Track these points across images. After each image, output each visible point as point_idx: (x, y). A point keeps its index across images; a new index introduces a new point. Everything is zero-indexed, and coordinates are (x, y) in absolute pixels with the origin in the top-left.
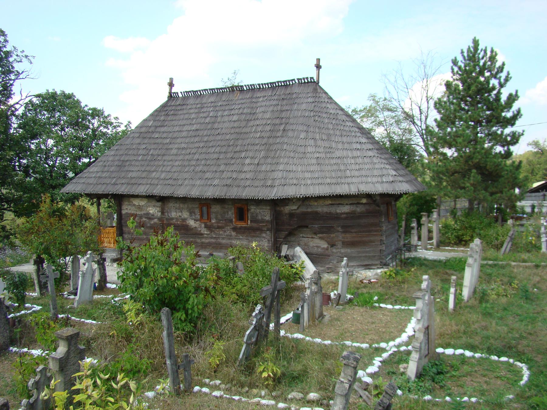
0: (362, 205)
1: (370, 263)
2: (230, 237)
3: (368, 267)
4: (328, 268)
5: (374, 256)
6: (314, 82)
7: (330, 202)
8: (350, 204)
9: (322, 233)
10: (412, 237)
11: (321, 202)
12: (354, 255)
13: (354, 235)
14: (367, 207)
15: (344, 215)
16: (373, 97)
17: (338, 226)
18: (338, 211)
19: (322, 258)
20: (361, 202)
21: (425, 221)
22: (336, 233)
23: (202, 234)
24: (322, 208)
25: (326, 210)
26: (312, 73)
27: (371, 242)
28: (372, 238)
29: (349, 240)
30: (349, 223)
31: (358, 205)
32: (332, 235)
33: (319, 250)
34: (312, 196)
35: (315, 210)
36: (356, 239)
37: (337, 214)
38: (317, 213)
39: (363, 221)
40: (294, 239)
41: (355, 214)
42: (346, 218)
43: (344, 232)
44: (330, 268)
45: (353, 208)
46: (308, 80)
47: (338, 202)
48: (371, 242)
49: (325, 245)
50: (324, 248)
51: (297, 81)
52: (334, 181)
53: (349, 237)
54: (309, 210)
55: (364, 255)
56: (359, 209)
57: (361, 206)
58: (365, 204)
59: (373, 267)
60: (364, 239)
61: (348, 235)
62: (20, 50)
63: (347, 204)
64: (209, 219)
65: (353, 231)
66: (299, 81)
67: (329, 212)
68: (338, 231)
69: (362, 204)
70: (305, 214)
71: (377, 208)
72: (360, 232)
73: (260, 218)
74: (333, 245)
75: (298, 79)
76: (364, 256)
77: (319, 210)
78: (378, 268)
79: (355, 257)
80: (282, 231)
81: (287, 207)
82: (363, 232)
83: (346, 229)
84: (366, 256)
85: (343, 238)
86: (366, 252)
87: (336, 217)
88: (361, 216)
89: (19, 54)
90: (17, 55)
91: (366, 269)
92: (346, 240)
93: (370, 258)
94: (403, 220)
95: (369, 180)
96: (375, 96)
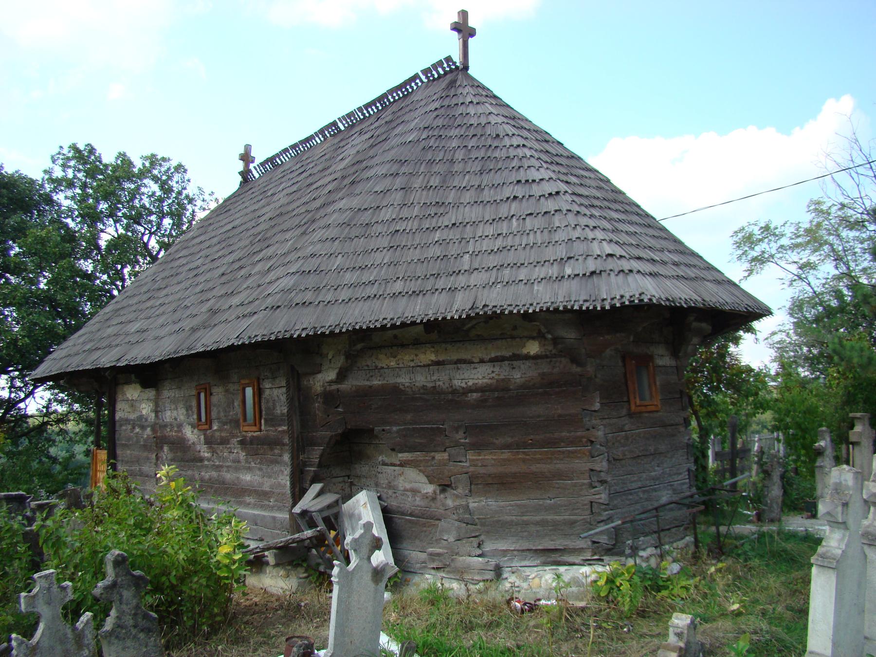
0: (528, 363)
1: (559, 543)
2: (237, 466)
3: (552, 556)
4: (431, 554)
5: (572, 523)
6: (457, 68)
7: (433, 357)
8: (492, 360)
9: (412, 449)
10: (818, 476)
11: (407, 358)
12: (508, 518)
13: (506, 455)
14: (545, 367)
15: (475, 395)
16: (817, 207)
17: (457, 429)
18: (457, 383)
19: (424, 525)
20: (525, 351)
21: (860, 434)
22: (453, 451)
23: (201, 460)
24: (411, 372)
25: (421, 379)
26: (451, 47)
27: (559, 475)
28: (560, 466)
29: (492, 470)
30: (492, 418)
31: (515, 363)
32: (439, 456)
33: (418, 501)
34: (332, 332)
35: (392, 381)
36: (514, 469)
37: (454, 392)
38: (395, 390)
39: (537, 410)
40: (367, 468)
41: (507, 389)
42: (481, 404)
43: (477, 447)
44: (439, 555)
45: (499, 372)
46: (444, 69)
47: (455, 357)
48: (559, 475)
49: (429, 489)
50: (425, 496)
51: (423, 78)
52: (413, 286)
53: (490, 460)
54: (376, 382)
55: (538, 518)
56: (519, 375)
57: (524, 366)
58: (536, 357)
59: (571, 559)
60: (535, 468)
61: (488, 457)
62: (207, 191)
63: (482, 361)
64: (209, 422)
65: (500, 441)
66: (427, 77)
67: (430, 385)
68: (457, 445)
69: (527, 357)
70: (364, 395)
71: (576, 369)
72: (525, 445)
73: (279, 412)
74: (445, 487)
75: (426, 72)
76: (537, 523)
77: (404, 380)
78: (587, 562)
79: (511, 524)
80: (315, 445)
81: (319, 376)
82: (532, 446)
83: (480, 436)
84: (543, 523)
85: (473, 464)
86: (548, 509)
87: (454, 399)
88: (524, 395)
89: (207, 197)
90: (203, 200)
91: (545, 564)
92: (482, 470)
93: (556, 528)
94: (437, 356)
95: (523, 274)
96: (818, 203)
